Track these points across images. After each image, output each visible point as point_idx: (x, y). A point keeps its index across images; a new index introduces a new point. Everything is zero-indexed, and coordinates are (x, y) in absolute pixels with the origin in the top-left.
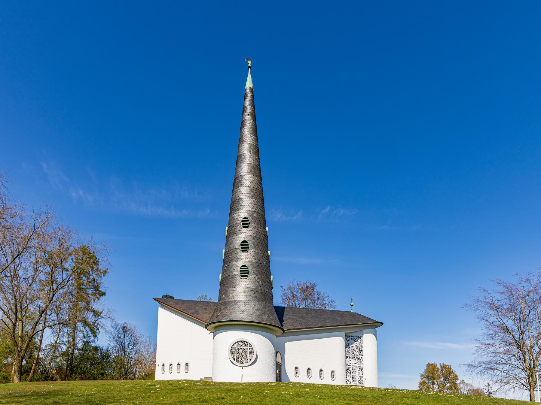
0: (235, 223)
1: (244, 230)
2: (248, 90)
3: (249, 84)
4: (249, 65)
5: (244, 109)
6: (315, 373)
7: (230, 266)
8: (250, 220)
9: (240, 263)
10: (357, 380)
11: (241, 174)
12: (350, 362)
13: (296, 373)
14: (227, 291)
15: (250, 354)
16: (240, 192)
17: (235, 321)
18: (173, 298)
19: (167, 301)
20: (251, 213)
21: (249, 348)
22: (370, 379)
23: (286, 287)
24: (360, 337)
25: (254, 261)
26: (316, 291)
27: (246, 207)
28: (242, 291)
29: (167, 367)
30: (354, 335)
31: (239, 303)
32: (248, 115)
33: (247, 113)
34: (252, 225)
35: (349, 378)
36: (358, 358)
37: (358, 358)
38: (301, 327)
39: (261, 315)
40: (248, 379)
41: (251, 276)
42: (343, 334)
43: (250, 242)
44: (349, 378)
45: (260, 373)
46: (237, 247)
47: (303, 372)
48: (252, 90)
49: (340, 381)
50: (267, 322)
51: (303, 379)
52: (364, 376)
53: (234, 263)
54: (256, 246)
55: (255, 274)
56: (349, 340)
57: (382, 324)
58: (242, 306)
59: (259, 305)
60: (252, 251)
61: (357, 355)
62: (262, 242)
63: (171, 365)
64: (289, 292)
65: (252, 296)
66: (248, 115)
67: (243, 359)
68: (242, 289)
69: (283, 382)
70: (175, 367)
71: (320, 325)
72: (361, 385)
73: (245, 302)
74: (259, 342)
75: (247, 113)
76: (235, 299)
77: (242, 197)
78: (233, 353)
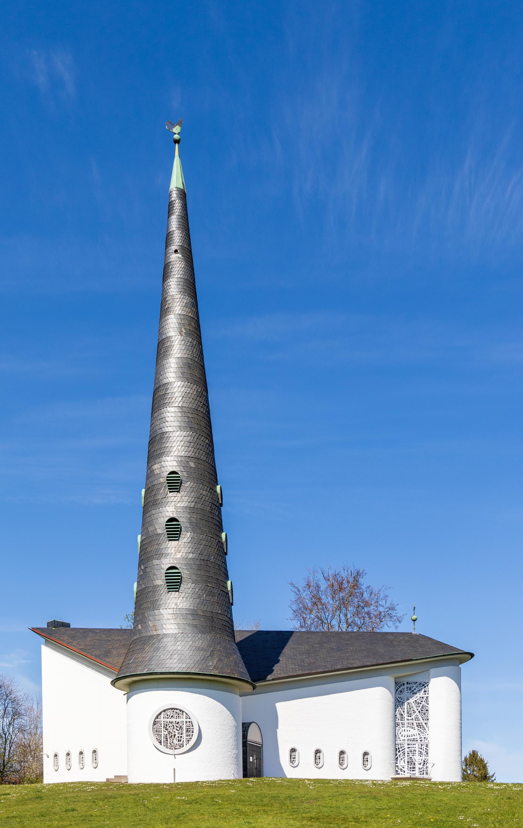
0: (156, 482)
1: (173, 497)
2: (174, 196)
3: (176, 181)
4: (176, 137)
5: (168, 239)
6: (330, 758)
7: (148, 570)
8: (183, 475)
9: (166, 563)
10: (417, 766)
11: (165, 381)
12: (403, 733)
13: (292, 759)
14: (144, 617)
15: (187, 731)
16: (163, 420)
17: (156, 673)
18: (68, 625)
19: (57, 633)
20: (184, 462)
21: (185, 720)
22: (444, 767)
23: (301, 584)
24: (424, 685)
25: (191, 556)
26: (364, 587)
27: (176, 452)
28: (170, 617)
29: (62, 758)
30: (410, 680)
31: (165, 640)
32: (176, 251)
33: (174, 248)
34: (187, 485)
35: (402, 763)
36: (419, 725)
37: (419, 725)
38: (300, 672)
39: (205, 659)
40: (182, 778)
41: (187, 587)
42: (390, 680)
43: (183, 521)
44: (402, 763)
45: (212, 762)
46: (159, 531)
47: (306, 756)
48: (183, 195)
49: (380, 771)
50: (216, 672)
51: (304, 770)
52: (431, 759)
53: (155, 562)
54: (195, 527)
55: (195, 582)
56: (403, 691)
57: (472, 655)
58: (169, 645)
59: (202, 641)
60: (186, 537)
61: (417, 719)
62: (210, 516)
63: (68, 754)
64: (306, 595)
65: (189, 625)
66: (176, 251)
67: (176, 742)
68: (171, 611)
69: (266, 779)
70: (75, 756)
71: (339, 667)
72: (425, 776)
73: (175, 636)
74: (203, 709)
75: (174, 248)
76: (159, 632)
77: (167, 430)
78: (156, 732)
